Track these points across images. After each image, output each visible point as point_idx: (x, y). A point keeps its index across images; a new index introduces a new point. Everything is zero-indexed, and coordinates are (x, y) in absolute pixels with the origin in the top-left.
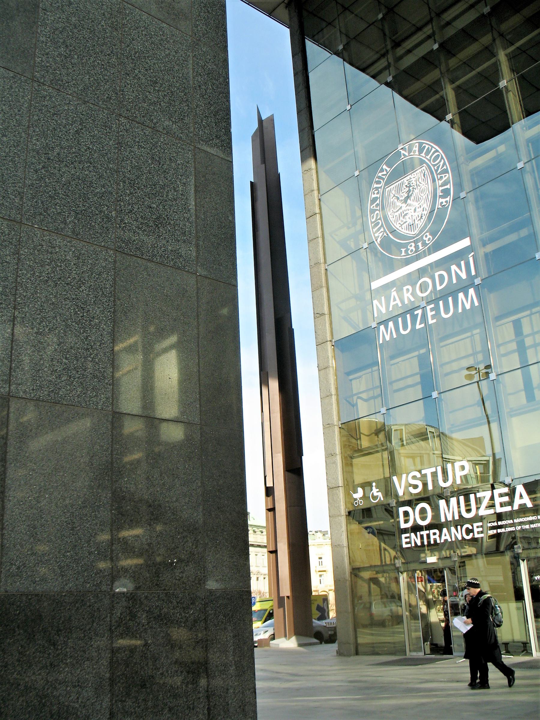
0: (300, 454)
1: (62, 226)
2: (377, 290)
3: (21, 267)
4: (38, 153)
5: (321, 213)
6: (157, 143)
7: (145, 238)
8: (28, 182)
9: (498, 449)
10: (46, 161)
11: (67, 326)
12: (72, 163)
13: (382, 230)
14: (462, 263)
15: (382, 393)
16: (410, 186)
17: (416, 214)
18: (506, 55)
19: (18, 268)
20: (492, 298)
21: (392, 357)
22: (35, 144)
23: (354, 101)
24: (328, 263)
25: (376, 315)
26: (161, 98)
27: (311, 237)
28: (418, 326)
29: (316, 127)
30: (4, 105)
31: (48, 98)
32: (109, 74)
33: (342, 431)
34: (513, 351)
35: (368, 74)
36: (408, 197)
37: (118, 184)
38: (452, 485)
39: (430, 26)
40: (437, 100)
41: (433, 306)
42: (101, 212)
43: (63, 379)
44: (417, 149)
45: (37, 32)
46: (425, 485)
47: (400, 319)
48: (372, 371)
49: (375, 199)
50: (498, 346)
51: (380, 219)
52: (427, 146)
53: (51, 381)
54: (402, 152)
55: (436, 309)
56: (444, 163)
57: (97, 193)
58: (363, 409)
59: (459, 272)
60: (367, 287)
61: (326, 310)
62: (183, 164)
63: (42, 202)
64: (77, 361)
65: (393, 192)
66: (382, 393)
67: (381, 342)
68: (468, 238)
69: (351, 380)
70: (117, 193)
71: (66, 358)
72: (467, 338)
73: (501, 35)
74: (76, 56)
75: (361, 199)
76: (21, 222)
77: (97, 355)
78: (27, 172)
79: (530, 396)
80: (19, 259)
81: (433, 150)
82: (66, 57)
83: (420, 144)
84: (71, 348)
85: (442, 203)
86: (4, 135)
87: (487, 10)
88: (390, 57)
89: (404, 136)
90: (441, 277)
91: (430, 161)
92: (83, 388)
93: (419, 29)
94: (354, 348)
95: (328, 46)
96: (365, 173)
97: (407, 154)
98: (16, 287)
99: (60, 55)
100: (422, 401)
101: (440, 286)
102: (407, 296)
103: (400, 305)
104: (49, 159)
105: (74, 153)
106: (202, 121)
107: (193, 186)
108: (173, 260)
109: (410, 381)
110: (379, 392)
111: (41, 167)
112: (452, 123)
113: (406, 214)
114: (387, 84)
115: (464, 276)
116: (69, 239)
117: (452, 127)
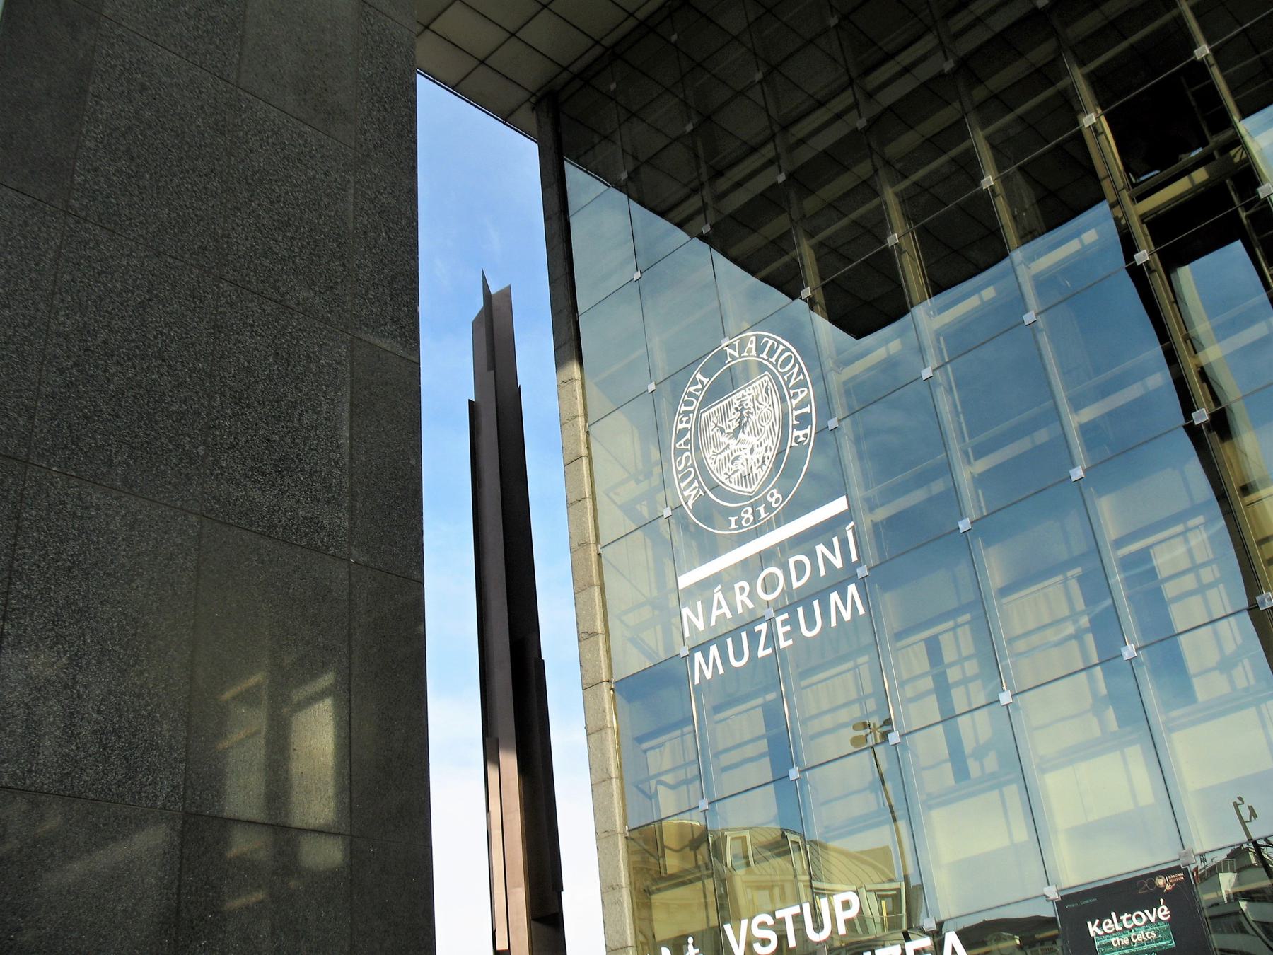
0: (558, 887)
1: (105, 470)
2: (690, 590)
3: (22, 543)
4: (67, 339)
5: (589, 457)
6: (284, 327)
7: (254, 494)
8: (45, 390)
9: (911, 870)
10: (81, 353)
11: (103, 652)
12: (129, 359)
13: (696, 484)
14: (835, 540)
15: (699, 773)
16: (743, 409)
17: (755, 457)
18: (896, 194)
19: (15, 544)
20: (888, 601)
21: (717, 709)
22: (64, 324)
23: (648, 265)
24: (603, 542)
25: (687, 634)
26: (296, 250)
27: (573, 498)
28: (762, 653)
29: (582, 306)
30: (10, 253)
31: (91, 245)
32: (204, 207)
33: (631, 843)
34: (928, 693)
35: (669, 220)
36: (740, 428)
37: (211, 398)
38: (831, 937)
39: (770, 146)
40: (787, 265)
41: (786, 616)
42: (178, 446)
43: (90, 751)
44: (754, 346)
45: (81, 133)
46: (782, 938)
47: (729, 641)
48: (682, 735)
49: (682, 432)
50: (902, 684)
51: (692, 465)
52: (771, 342)
53: (67, 755)
54: (729, 351)
55: (793, 620)
56: (796, 370)
57: (173, 412)
58: (667, 803)
59: (830, 556)
60: (671, 584)
61: (599, 626)
62: (330, 366)
63: (69, 427)
64: (120, 717)
65: (714, 419)
66: (699, 773)
67: (697, 681)
68: (844, 498)
69: (645, 751)
70: (208, 414)
71: (99, 712)
72: (848, 671)
73: (888, 163)
74: (147, 176)
75: (658, 433)
76: (27, 461)
77: (158, 705)
78: (44, 373)
79: (961, 772)
80: (18, 527)
81: (781, 347)
82: (129, 176)
83: (759, 338)
84: (110, 692)
85: (798, 437)
86: (4, 306)
87: (861, 123)
88: (706, 192)
89: (731, 325)
90: (800, 567)
91: (775, 366)
92: (129, 768)
93: (754, 149)
94: (651, 694)
95: (602, 173)
96: (667, 386)
97: (736, 354)
98: (10, 578)
99: (119, 171)
100: (772, 786)
101: (798, 580)
102: (742, 599)
103: (729, 616)
104: (86, 350)
105: (133, 341)
106: (367, 292)
107: (347, 406)
108: (306, 534)
109: (750, 751)
110: (696, 772)
111: (71, 363)
112: (811, 302)
113: (737, 458)
114: (703, 238)
115: (838, 562)
116: (115, 494)
117: (812, 308)
